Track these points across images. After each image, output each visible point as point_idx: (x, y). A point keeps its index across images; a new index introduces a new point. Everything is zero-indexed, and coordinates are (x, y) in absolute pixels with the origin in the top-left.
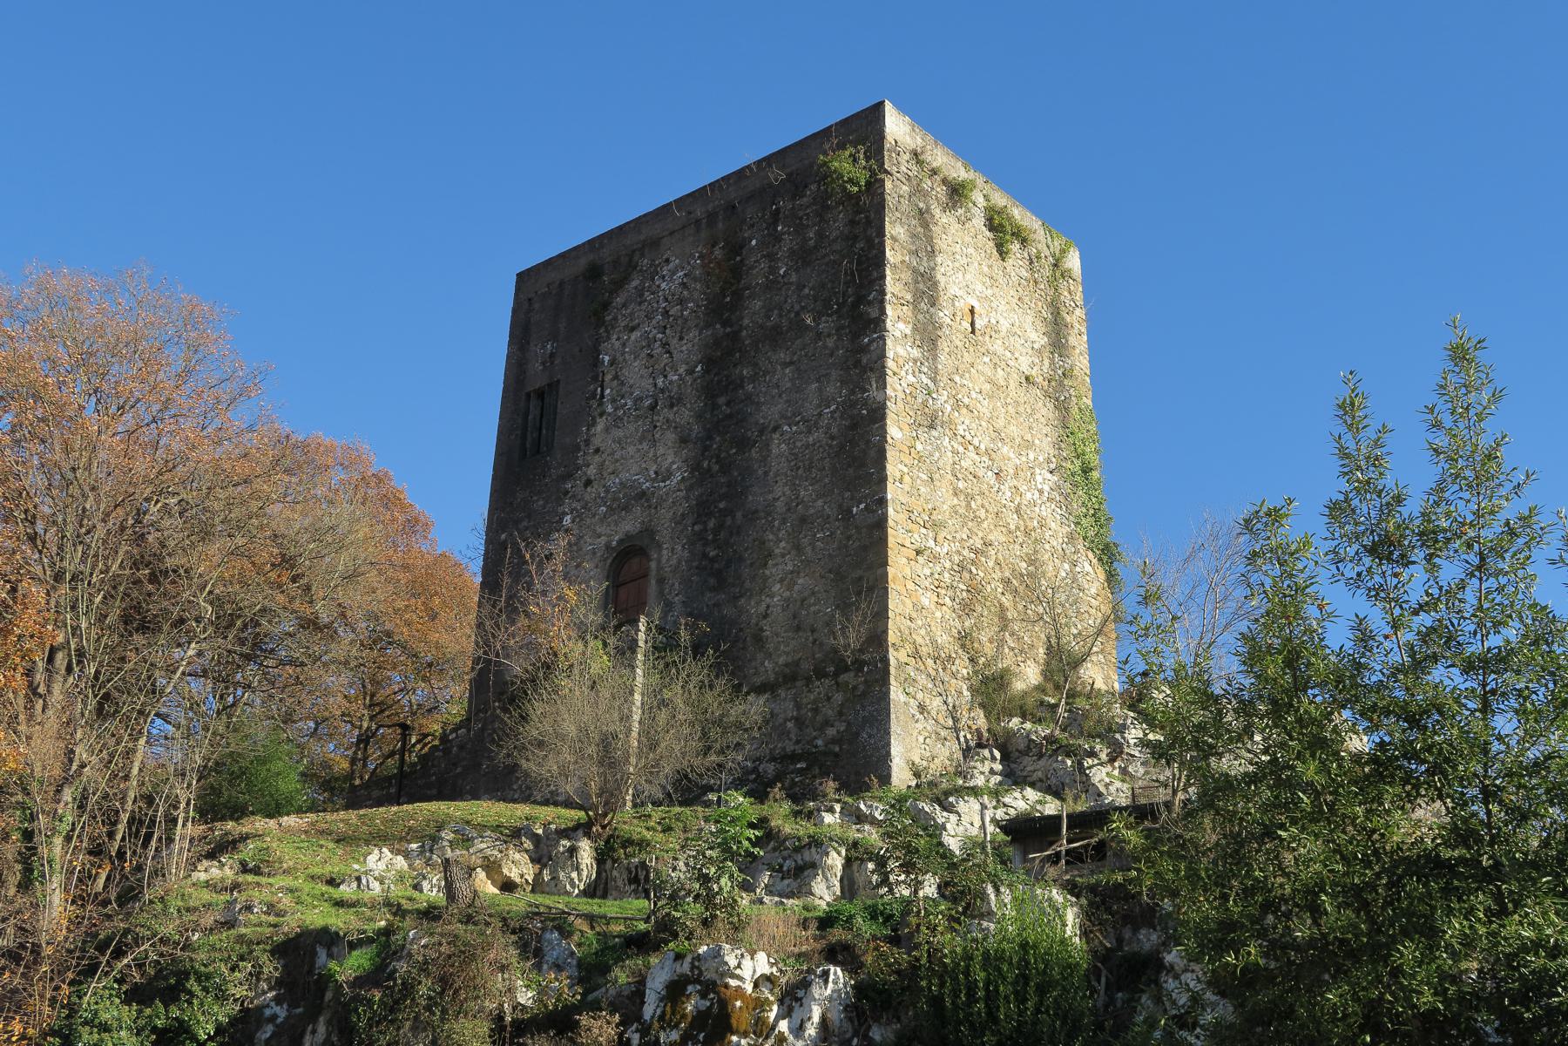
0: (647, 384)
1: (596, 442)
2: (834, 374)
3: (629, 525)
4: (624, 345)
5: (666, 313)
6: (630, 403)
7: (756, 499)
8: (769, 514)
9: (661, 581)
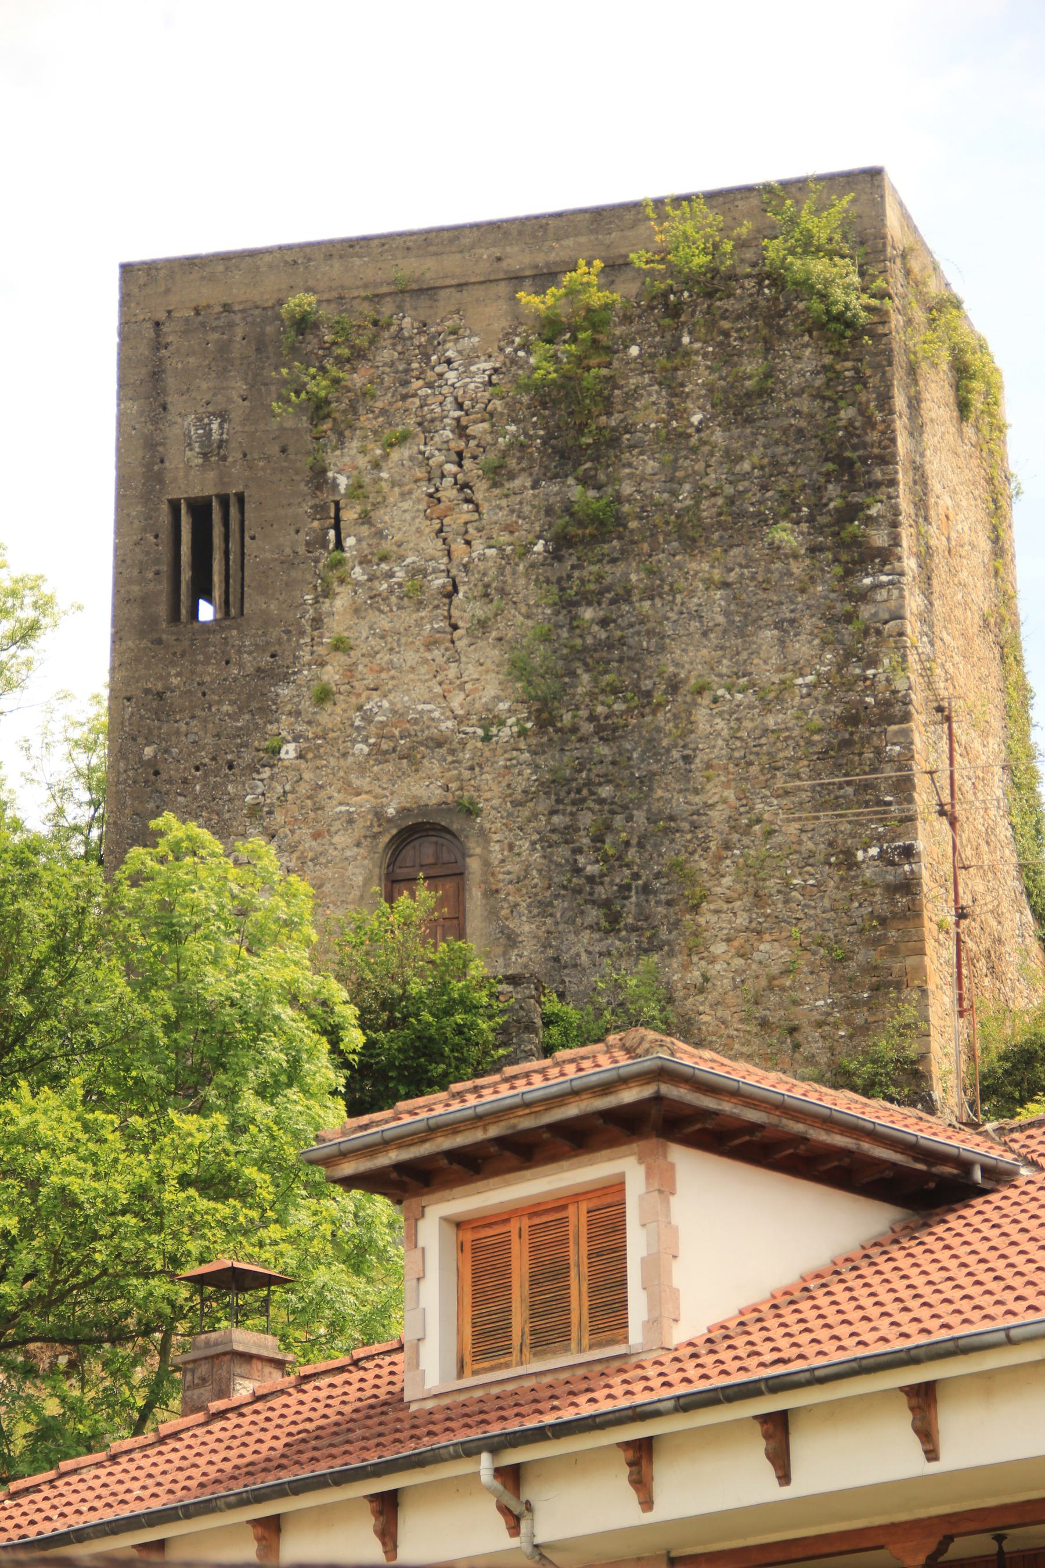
0: (433, 546)
2: (808, 623)
3: (424, 788)
4: (377, 466)
5: (461, 430)
6: (400, 575)
7: (668, 795)
8: (695, 827)
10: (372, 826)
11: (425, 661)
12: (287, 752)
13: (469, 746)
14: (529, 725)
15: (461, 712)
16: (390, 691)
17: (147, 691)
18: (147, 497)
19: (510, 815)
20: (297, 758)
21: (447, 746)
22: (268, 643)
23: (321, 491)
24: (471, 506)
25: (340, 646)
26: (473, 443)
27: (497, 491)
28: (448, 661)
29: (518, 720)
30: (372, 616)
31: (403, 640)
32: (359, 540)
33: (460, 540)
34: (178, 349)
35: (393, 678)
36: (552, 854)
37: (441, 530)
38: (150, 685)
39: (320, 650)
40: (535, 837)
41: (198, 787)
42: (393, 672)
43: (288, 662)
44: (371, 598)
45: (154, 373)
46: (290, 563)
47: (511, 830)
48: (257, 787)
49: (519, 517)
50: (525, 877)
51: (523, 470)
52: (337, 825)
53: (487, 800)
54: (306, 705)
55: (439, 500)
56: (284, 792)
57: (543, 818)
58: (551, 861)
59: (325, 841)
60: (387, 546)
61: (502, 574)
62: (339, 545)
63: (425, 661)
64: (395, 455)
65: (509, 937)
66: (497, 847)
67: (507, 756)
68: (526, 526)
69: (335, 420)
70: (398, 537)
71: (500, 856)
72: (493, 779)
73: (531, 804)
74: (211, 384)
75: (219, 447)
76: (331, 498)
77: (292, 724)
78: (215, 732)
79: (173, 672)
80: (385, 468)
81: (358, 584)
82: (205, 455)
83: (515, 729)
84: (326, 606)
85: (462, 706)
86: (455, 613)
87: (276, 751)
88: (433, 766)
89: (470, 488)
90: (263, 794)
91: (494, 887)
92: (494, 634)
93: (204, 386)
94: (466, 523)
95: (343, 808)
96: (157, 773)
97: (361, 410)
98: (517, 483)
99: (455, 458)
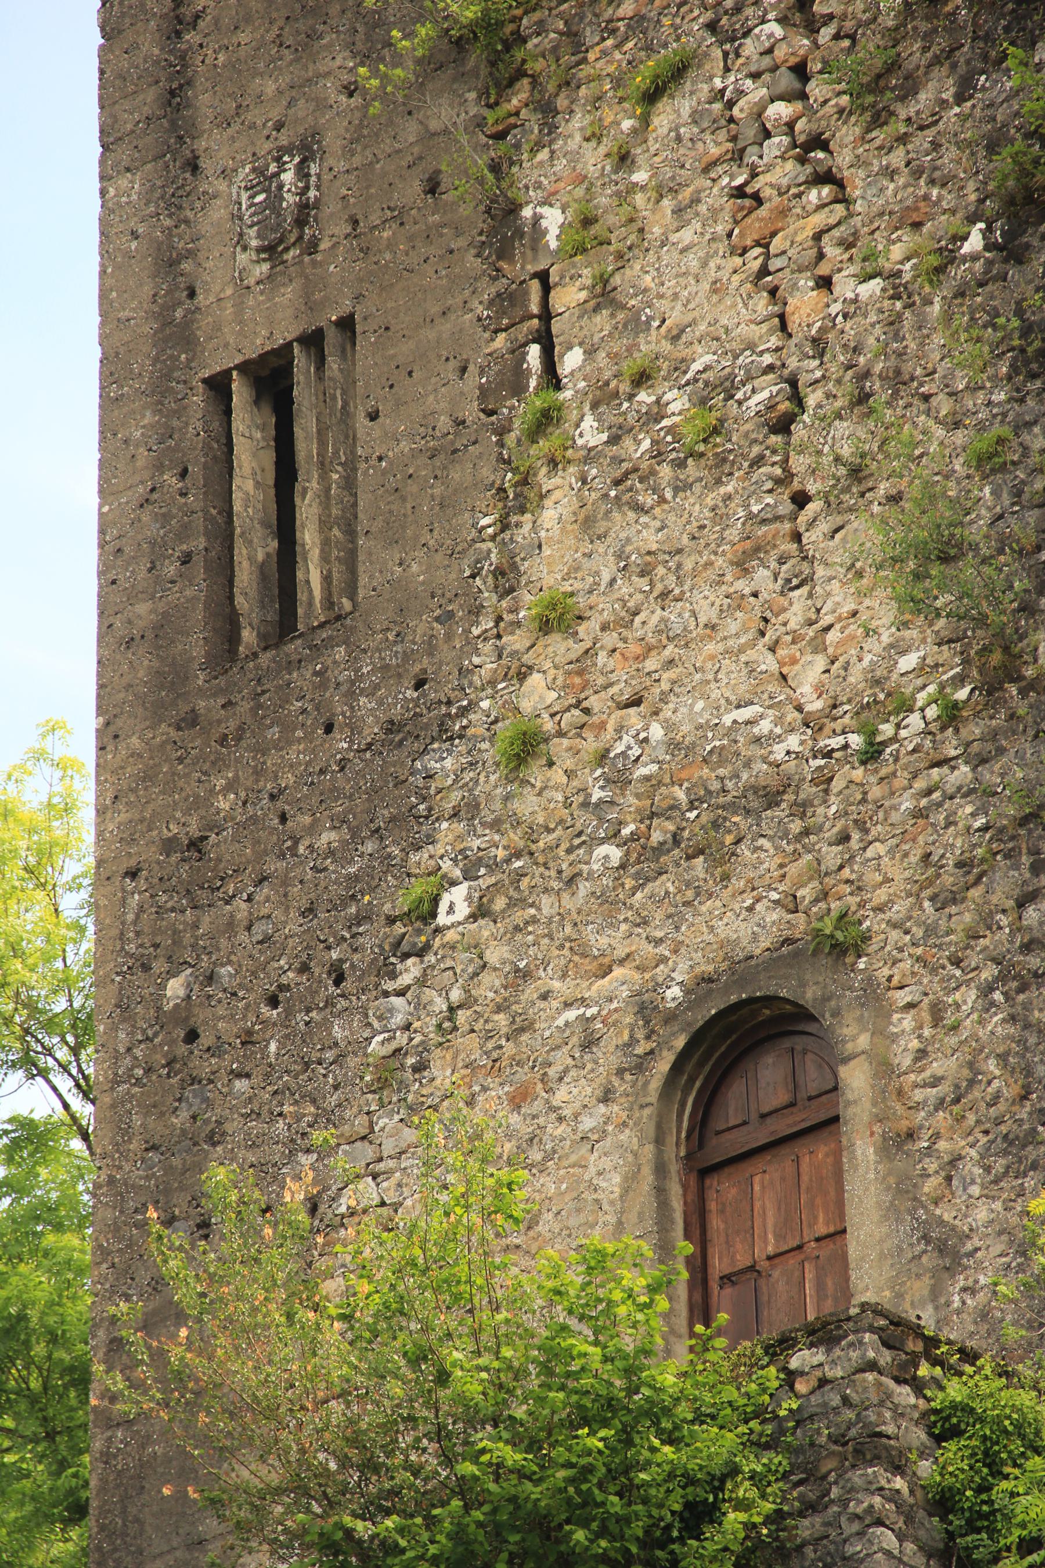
0: (745, 316)
1: (546, 574)
3: (737, 922)
4: (624, 159)
6: (677, 402)
9: (899, 1142)
10: (633, 1041)
11: (737, 601)
12: (451, 910)
13: (837, 785)
14: (962, 694)
15: (815, 705)
16: (664, 699)
17: (169, 845)
18: (162, 390)
19: (930, 930)
20: (473, 917)
21: (790, 797)
22: (406, 656)
23: (511, 260)
24: (826, 190)
25: (557, 619)
26: (826, 34)
27: (880, 136)
28: (789, 586)
29: (942, 687)
30: (623, 526)
31: (688, 565)
32: (590, 353)
33: (806, 282)
34: (216, 21)
35: (671, 663)
36: (1027, 1006)
37: (764, 271)
38: (174, 829)
39: (515, 641)
40: (989, 972)
41: (273, 1047)
42: (670, 651)
43: (448, 690)
44: (617, 483)
45: (172, 93)
46: (446, 453)
47: (934, 971)
48: (391, 1010)
49: (932, 182)
50: (972, 1083)
51: (936, 61)
52: (561, 1059)
53: (879, 909)
54: (491, 783)
55: (758, 199)
56: (452, 1009)
57: (1004, 920)
58: (1027, 1026)
59: (538, 1106)
60: (651, 344)
61: (897, 337)
62: (552, 377)
63: (737, 601)
64: (665, 117)
65: (942, 1249)
66: (908, 1022)
67: (920, 784)
68: (949, 200)
69: (534, 79)
70: (676, 316)
71: (915, 1044)
72: (891, 852)
73: (975, 893)
74: (284, 81)
75: (301, 222)
76: (531, 268)
77: (460, 838)
78: (304, 904)
79: (220, 783)
80: (641, 160)
81: (591, 455)
82: (271, 251)
83: (932, 712)
84: (523, 534)
85: (820, 691)
86: (799, 463)
87: (426, 912)
88: (761, 857)
89: (825, 146)
90: (407, 1027)
91: (904, 1125)
92: (883, 488)
93: (270, 88)
94: (818, 237)
95: (571, 1015)
96: (192, 1036)
97: (590, 36)
98: (925, 97)
99: (786, 80)
